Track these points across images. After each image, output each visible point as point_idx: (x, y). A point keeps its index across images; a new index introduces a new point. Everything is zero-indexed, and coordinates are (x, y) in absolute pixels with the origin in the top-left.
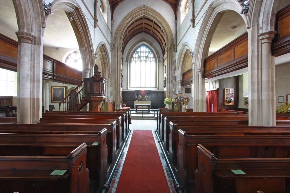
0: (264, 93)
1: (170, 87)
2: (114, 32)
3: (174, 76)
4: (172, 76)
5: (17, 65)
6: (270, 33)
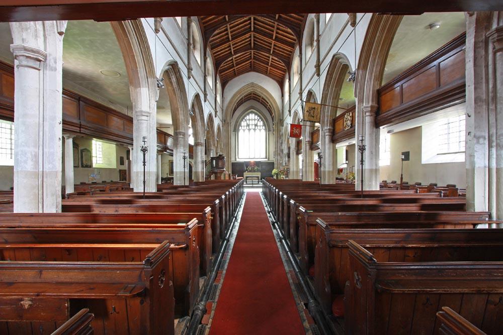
0: (308, 168)
2: (225, 109)
4: (280, 149)
5: (133, 139)
6: (329, 129)
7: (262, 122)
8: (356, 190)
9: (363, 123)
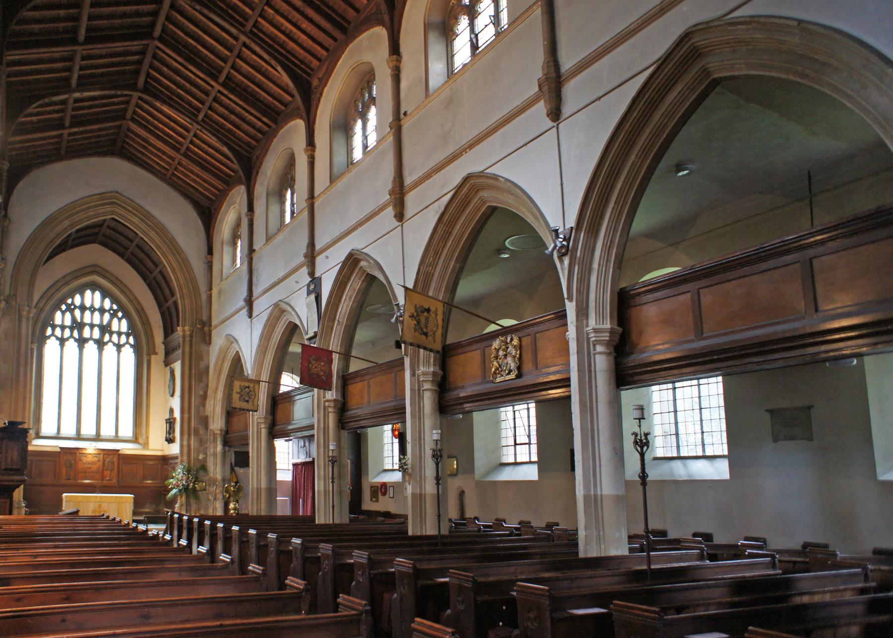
1: (189, 446)
3: (201, 415)
4: (197, 413)
6: (335, 401)
7: (124, 322)
8: (582, 555)
9: (590, 371)
